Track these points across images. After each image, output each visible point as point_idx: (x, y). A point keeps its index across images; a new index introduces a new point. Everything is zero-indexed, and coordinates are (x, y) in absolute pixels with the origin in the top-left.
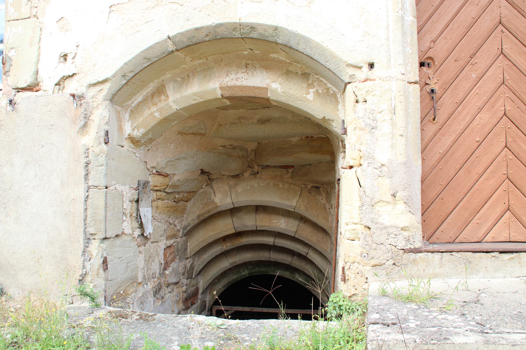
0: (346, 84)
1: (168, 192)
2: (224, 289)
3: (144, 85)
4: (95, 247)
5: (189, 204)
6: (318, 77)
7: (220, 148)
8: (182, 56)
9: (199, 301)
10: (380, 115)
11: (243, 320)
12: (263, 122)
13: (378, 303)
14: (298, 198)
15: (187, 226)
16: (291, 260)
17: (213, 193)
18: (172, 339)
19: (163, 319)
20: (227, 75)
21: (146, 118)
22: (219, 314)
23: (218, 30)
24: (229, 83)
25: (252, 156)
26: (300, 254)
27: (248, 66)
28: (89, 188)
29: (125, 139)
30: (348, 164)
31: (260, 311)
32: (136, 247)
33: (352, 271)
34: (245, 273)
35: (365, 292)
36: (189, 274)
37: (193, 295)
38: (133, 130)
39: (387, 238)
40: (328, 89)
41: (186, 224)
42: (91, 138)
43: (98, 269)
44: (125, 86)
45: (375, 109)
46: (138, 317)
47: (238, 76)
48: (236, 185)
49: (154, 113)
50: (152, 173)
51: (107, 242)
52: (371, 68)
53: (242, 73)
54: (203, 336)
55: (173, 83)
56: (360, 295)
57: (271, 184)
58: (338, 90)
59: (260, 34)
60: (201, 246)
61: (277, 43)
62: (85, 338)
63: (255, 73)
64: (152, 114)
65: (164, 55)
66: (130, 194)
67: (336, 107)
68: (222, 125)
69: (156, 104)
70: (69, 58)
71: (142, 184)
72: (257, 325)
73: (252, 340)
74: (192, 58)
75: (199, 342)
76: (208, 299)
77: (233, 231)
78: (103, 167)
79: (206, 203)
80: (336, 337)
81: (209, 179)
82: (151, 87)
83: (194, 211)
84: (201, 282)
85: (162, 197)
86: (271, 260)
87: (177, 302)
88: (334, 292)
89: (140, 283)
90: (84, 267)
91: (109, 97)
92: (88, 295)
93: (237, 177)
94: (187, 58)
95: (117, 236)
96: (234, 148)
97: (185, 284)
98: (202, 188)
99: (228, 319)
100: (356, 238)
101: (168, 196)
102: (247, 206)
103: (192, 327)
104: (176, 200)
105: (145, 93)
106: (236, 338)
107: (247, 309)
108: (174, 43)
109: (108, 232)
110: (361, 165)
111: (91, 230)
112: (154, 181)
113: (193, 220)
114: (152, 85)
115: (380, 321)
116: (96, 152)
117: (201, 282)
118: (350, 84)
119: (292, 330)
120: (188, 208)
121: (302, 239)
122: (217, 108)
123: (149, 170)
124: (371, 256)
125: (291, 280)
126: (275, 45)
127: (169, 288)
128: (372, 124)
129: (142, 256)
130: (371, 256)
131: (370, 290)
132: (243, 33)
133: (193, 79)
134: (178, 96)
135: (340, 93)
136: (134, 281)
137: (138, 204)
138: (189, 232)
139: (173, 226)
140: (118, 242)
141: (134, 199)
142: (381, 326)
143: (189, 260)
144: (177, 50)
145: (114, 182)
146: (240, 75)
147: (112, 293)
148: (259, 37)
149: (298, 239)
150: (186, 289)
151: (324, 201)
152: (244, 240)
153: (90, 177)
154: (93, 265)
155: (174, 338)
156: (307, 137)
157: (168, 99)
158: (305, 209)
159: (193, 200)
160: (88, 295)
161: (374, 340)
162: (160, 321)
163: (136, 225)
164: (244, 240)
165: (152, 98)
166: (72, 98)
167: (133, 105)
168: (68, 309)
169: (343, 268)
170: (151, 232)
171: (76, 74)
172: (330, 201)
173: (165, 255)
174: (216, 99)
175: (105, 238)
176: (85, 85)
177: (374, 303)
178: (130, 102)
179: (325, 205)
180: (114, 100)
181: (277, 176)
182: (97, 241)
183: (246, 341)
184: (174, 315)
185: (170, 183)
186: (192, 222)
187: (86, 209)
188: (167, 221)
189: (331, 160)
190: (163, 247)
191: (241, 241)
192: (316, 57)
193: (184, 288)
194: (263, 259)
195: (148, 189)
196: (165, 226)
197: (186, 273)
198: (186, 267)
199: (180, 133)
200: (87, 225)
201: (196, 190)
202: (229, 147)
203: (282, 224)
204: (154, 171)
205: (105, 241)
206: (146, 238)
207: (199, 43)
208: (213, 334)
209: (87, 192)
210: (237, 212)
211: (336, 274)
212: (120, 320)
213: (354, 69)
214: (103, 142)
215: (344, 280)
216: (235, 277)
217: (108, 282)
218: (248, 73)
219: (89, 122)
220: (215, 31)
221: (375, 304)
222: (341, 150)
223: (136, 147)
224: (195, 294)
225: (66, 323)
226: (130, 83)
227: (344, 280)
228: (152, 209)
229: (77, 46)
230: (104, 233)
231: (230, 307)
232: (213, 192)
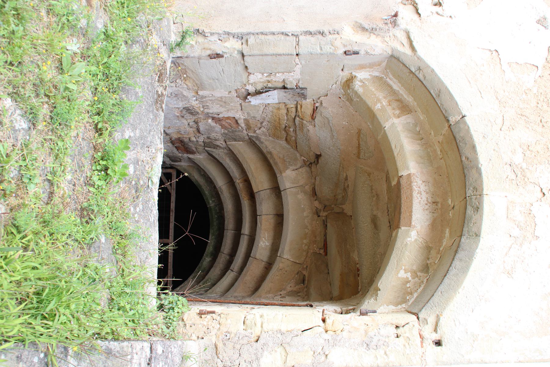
0: (416, 315)
3: (411, 90)
4: (234, 45)
5: (283, 143)
6: (425, 282)
7: (345, 175)
8: (444, 132)
9: (180, 155)
10: (382, 352)
11: (158, 204)
12: (374, 221)
13: (175, 352)
14: (292, 260)
15: (260, 141)
16: (225, 252)
17: (295, 168)
18: (136, 129)
19: (158, 119)
20: (423, 182)
21: (375, 94)
23: (474, 171)
24: (415, 184)
25: (337, 210)
26: (232, 263)
27: (434, 204)
28: (297, 36)
29: (350, 72)
30: (327, 318)
32: (236, 88)
33: (210, 322)
34: (211, 203)
36: (209, 144)
37: (187, 148)
38: (361, 81)
39: (247, 361)
40: (411, 294)
41: (262, 140)
42: (350, 36)
43: (210, 49)
44: (408, 71)
45: (390, 348)
46: (160, 93)
47: (423, 193)
48: (305, 192)
49: (380, 103)
51: (239, 57)
52: (436, 343)
53: (427, 198)
54: (140, 163)
55: (414, 122)
56: (185, 331)
57: (307, 231)
58: (411, 305)
59: (471, 218)
60: (239, 156)
61: (461, 236)
62: (137, 39)
63: (427, 212)
64: (379, 100)
65: (444, 112)
67: (391, 303)
68: (370, 176)
69: (390, 105)
70: (437, 8)
71: (303, 92)
72: (152, 220)
73: (136, 215)
74: (442, 142)
75: (134, 159)
76: (183, 164)
77: (255, 190)
78: (319, 51)
79: (285, 161)
80: (139, 306)
81: (311, 163)
82: (409, 99)
83: (276, 148)
85: (290, 114)
86: (225, 231)
87: (179, 132)
89: (197, 93)
90: (212, 34)
91: (396, 54)
92: (183, 39)
93: (314, 193)
94: (442, 137)
95: (246, 67)
96: (345, 190)
97: (198, 139)
98: (301, 156)
99: (159, 189)
100: (247, 326)
101: (291, 120)
102: (282, 205)
103: (150, 150)
104: (287, 128)
105: (401, 92)
106: (138, 197)
107: (173, 205)
108: (457, 123)
109: (250, 58)
110: (326, 331)
111: (252, 40)
112: (307, 105)
113: (266, 147)
114: (410, 100)
115: (154, 355)
116: (336, 42)
118: (416, 319)
119: (147, 258)
120: (279, 142)
121: (247, 265)
122: (388, 171)
123: (319, 98)
124: (227, 343)
126: (459, 234)
127: (193, 123)
128: (372, 344)
129: (225, 94)
130: (227, 343)
132: (471, 199)
133: (419, 144)
134: (400, 128)
135: (407, 307)
136: (199, 86)
137: (281, 89)
138: (253, 143)
139: (259, 125)
140: (240, 69)
141: (287, 84)
142: (149, 356)
143: (224, 143)
144: (450, 126)
145: (303, 62)
146: (424, 196)
147: (186, 64)
148: (467, 216)
149: (248, 260)
150: (193, 141)
151: (289, 289)
152: (245, 202)
153: (309, 37)
154: (215, 44)
155: (138, 131)
156: (358, 270)
157: (395, 117)
160: (183, 39)
161: (132, 349)
163: (259, 87)
164: (245, 202)
165: (396, 100)
166: (393, 14)
167: (388, 79)
168: (168, 20)
169: (213, 312)
170: (252, 103)
171: (420, 16)
172: (289, 296)
173: (228, 118)
174: (397, 171)
175: (243, 56)
176: (408, 28)
177: (175, 347)
178: (391, 76)
179: (284, 289)
180: (393, 59)
181: (315, 237)
182: (240, 47)
183: (135, 209)
185: (305, 122)
187: (274, 34)
188: (264, 119)
189: (334, 296)
190: (237, 116)
191: (245, 199)
192: (446, 280)
193: (193, 139)
194: (226, 222)
195: (298, 99)
197: (209, 140)
198: (216, 140)
199: (359, 132)
200: (257, 36)
201: (298, 150)
203: (264, 243)
204: (317, 105)
205: (240, 56)
206: (246, 98)
207: (459, 150)
208: (143, 173)
209: (292, 35)
210: (276, 195)
212: (157, 74)
213: (434, 324)
214: (346, 49)
217: (197, 60)
218: (426, 204)
219: (368, 33)
220: (472, 168)
222: (344, 309)
223: (342, 84)
224: (188, 150)
225: (152, 18)
226: (412, 75)
228: (276, 103)
229: (451, 17)
231: (175, 188)
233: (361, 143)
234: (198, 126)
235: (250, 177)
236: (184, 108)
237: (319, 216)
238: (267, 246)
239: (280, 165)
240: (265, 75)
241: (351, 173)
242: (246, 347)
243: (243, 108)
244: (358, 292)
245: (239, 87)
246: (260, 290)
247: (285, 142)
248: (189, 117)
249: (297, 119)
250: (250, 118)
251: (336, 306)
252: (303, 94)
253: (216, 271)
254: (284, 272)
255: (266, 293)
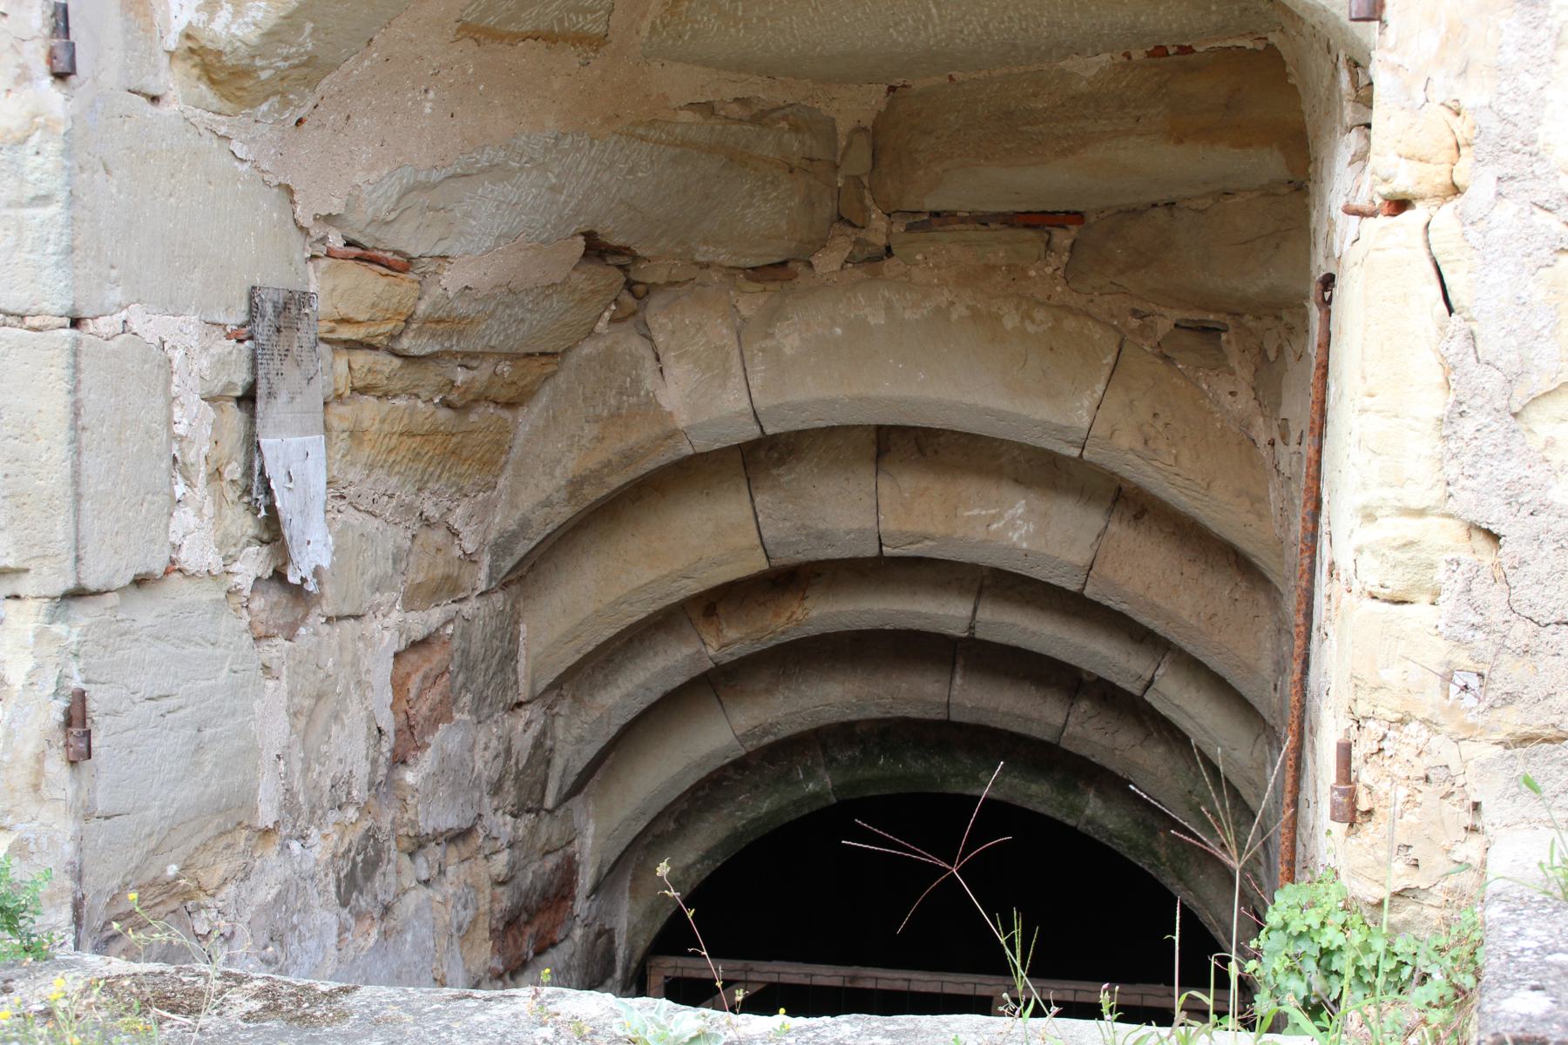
1: (415, 351)
2: (706, 870)
5: (527, 419)
7: (686, 116)
9: (578, 932)
13: (1542, 935)
14: (1100, 388)
16: (1060, 721)
17: (650, 363)
19: (391, 1011)
22: (691, 992)
25: (859, 161)
26: (1113, 686)
29: (165, 60)
30: (1385, 189)
31: (900, 985)
32: (247, 639)
33: (1396, 769)
34: (818, 784)
35: (1467, 880)
36: (527, 786)
37: (544, 897)
43: (40, 758)
46: (256, 1005)
48: (773, 315)
50: (321, 250)
51: (85, 615)
56: (1438, 897)
57: (960, 311)
66: (205, 363)
71: (269, 308)
76: (628, 922)
77: (756, 564)
78: (52, 210)
79: (615, 415)
81: (630, 285)
84: (591, 829)
85: (380, 379)
86: (956, 716)
87: (465, 934)
88: (1291, 878)
93: (774, 273)
95: (140, 582)
97: (503, 841)
98: (591, 333)
100: (1418, 587)
102: (830, 431)
104: (453, 397)
107: (827, 975)
109: (89, 558)
110: (1456, 190)
112: (339, 291)
113: (547, 503)
117: (591, 829)
120: (520, 440)
121: (1124, 607)
124: (1500, 686)
125: (1062, 825)
127: (420, 860)
129: (275, 692)
130: (1500, 686)
131: (1492, 871)
136: (232, 822)
137: (252, 415)
138: (529, 568)
139: (439, 536)
140: (146, 612)
141: (230, 385)
143: (525, 714)
145: (117, 295)
150: (512, 866)
151: (1243, 403)
156: (1159, 51)
158: (1139, 446)
159: (543, 399)
162: (375, 1022)
163: (247, 525)
164: (814, 613)
169: (1345, 752)
170: (325, 563)
173: (399, 685)
175: (78, 594)
179: (1247, 426)
181: (990, 269)
182: (32, 605)
184: (447, 992)
185: (422, 307)
186: (541, 512)
188: (408, 508)
190: (390, 642)
191: (799, 615)
193: (500, 863)
194: (913, 712)
195: (306, 335)
196: (397, 537)
197: (508, 784)
199: (472, 32)
201: (560, 346)
202: (736, 110)
205: (78, 609)
206: (298, 593)
210: (781, 462)
211: (1307, 793)
214: (41, 68)
215: (1352, 814)
216: (765, 806)
217: (93, 823)
221: (1521, 943)
222: (1349, 114)
223: (227, 107)
227: (1352, 814)
230: (70, 563)
232: (650, 355)
233: (527, 27)
234: (436, 837)
235: (693, 587)
236: (344, 904)
237: (889, 251)
238: (1030, 510)
239: (633, 438)
240: (180, 489)
241: (681, 84)
242: (1526, 592)
243: (346, 611)
244: (1272, 52)
245: (244, 624)
246: (1247, 547)
247: (523, 411)
248: (391, 879)
249: (405, 343)
250: (399, 579)
251: (1332, 156)
252: (282, 309)
253: (1150, 770)
254: (1159, 425)
255: (1260, 516)
